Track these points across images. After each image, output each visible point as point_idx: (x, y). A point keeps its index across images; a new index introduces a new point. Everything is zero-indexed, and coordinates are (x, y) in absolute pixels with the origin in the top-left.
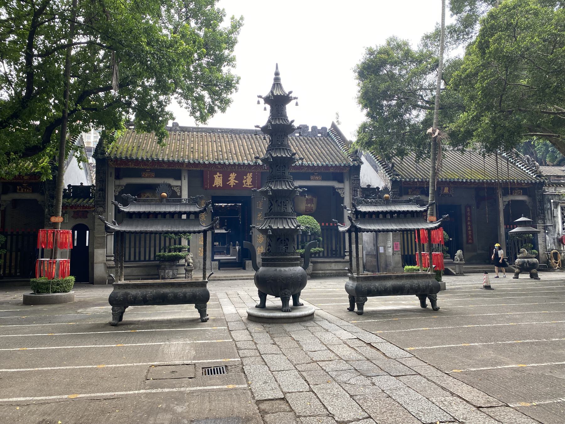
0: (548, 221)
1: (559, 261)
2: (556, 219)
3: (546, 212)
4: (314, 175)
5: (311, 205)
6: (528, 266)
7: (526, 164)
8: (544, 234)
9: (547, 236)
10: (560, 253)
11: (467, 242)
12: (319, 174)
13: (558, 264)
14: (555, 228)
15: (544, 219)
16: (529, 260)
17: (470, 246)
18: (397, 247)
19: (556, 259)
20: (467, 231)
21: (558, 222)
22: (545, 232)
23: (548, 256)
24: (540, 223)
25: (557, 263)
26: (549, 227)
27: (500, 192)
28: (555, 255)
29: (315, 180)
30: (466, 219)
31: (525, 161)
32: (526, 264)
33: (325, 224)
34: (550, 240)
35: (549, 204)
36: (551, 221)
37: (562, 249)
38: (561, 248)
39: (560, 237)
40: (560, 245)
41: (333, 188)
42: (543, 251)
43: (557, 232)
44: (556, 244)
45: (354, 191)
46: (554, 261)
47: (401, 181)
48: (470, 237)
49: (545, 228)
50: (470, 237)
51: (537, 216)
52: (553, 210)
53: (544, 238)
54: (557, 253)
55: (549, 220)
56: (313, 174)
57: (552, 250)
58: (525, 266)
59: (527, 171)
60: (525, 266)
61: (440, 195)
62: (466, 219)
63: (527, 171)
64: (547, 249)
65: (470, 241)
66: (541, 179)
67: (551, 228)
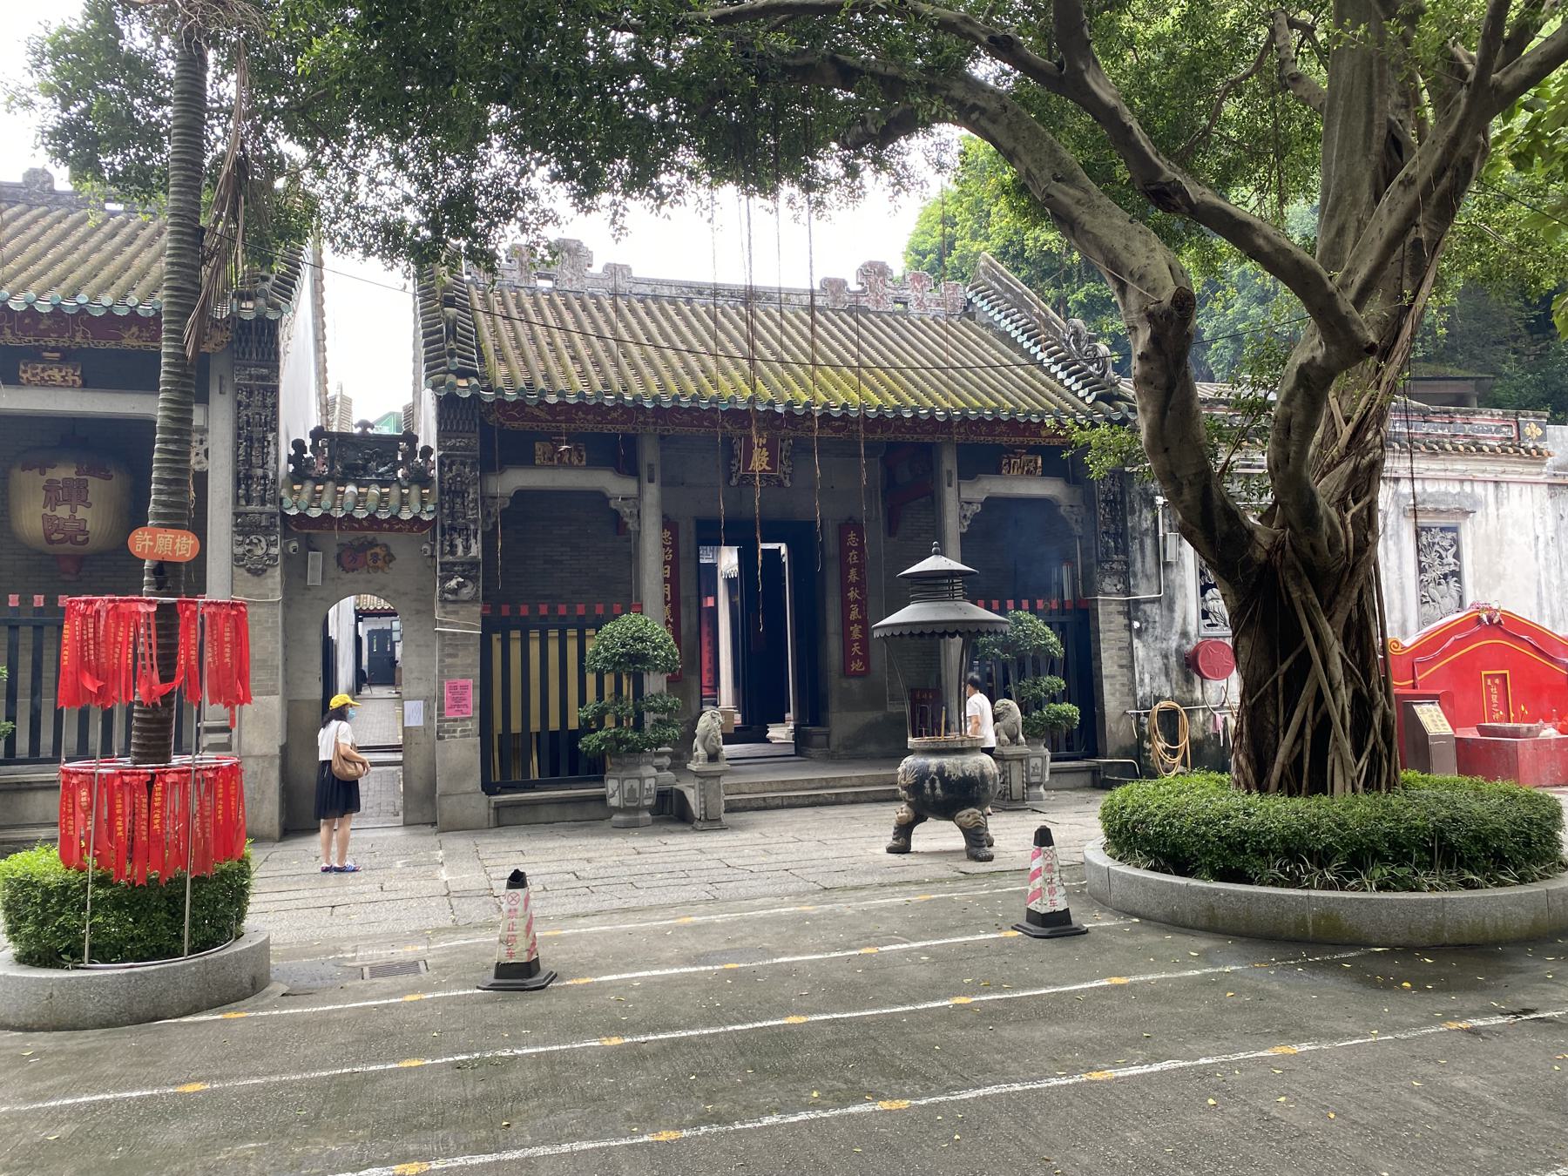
0: (1143, 584)
1: (1184, 742)
2: (1174, 575)
3: (1136, 546)
4: (43, 360)
5: (74, 511)
6: (938, 791)
7: (1070, 354)
8: (1127, 634)
9: (1136, 641)
10: (1190, 713)
11: (846, 673)
12: (67, 357)
13: (1179, 758)
14: (1171, 609)
15: (1125, 575)
16: (949, 762)
17: (855, 684)
18: (458, 703)
19: (1173, 738)
20: (846, 623)
21: (1183, 586)
22: (1129, 627)
23: (1140, 725)
24: (1108, 589)
25: (1174, 753)
26: (1147, 607)
27: (949, 463)
28: (1169, 720)
29: (44, 384)
30: (844, 574)
31: (1068, 344)
32: (933, 782)
33: (26, 600)
34: (1149, 659)
35: (1147, 514)
36: (1154, 581)
37: (1198, 694)
38: (1191, 691)
39: (1189, 648)
40: (1188, 680)
41: (599, 498)
42: (1122, 703)
43: (1178, 626)
44: (1174, 675)
45: (249, 439)
46: (1161, 745)
47: (475, 398)
48: (856, 649)
49: (1132, 609)
50: (856, 649)
51: (1099, 562)
52: (1165, 536)
53: (1125, 653)
54: (1175, 712)
55: (1148, 577)
56: (34, 355)
57: (1158, 699)
58: (928, 791)
59: (1067, 382)
60: (928, 791)
61: (734, 482)
62: (844, 574)
63: (1054, 369)
64: (1135, 695)
65: (856, 666)
66: (1117, 409)
67: (1153, 611)
